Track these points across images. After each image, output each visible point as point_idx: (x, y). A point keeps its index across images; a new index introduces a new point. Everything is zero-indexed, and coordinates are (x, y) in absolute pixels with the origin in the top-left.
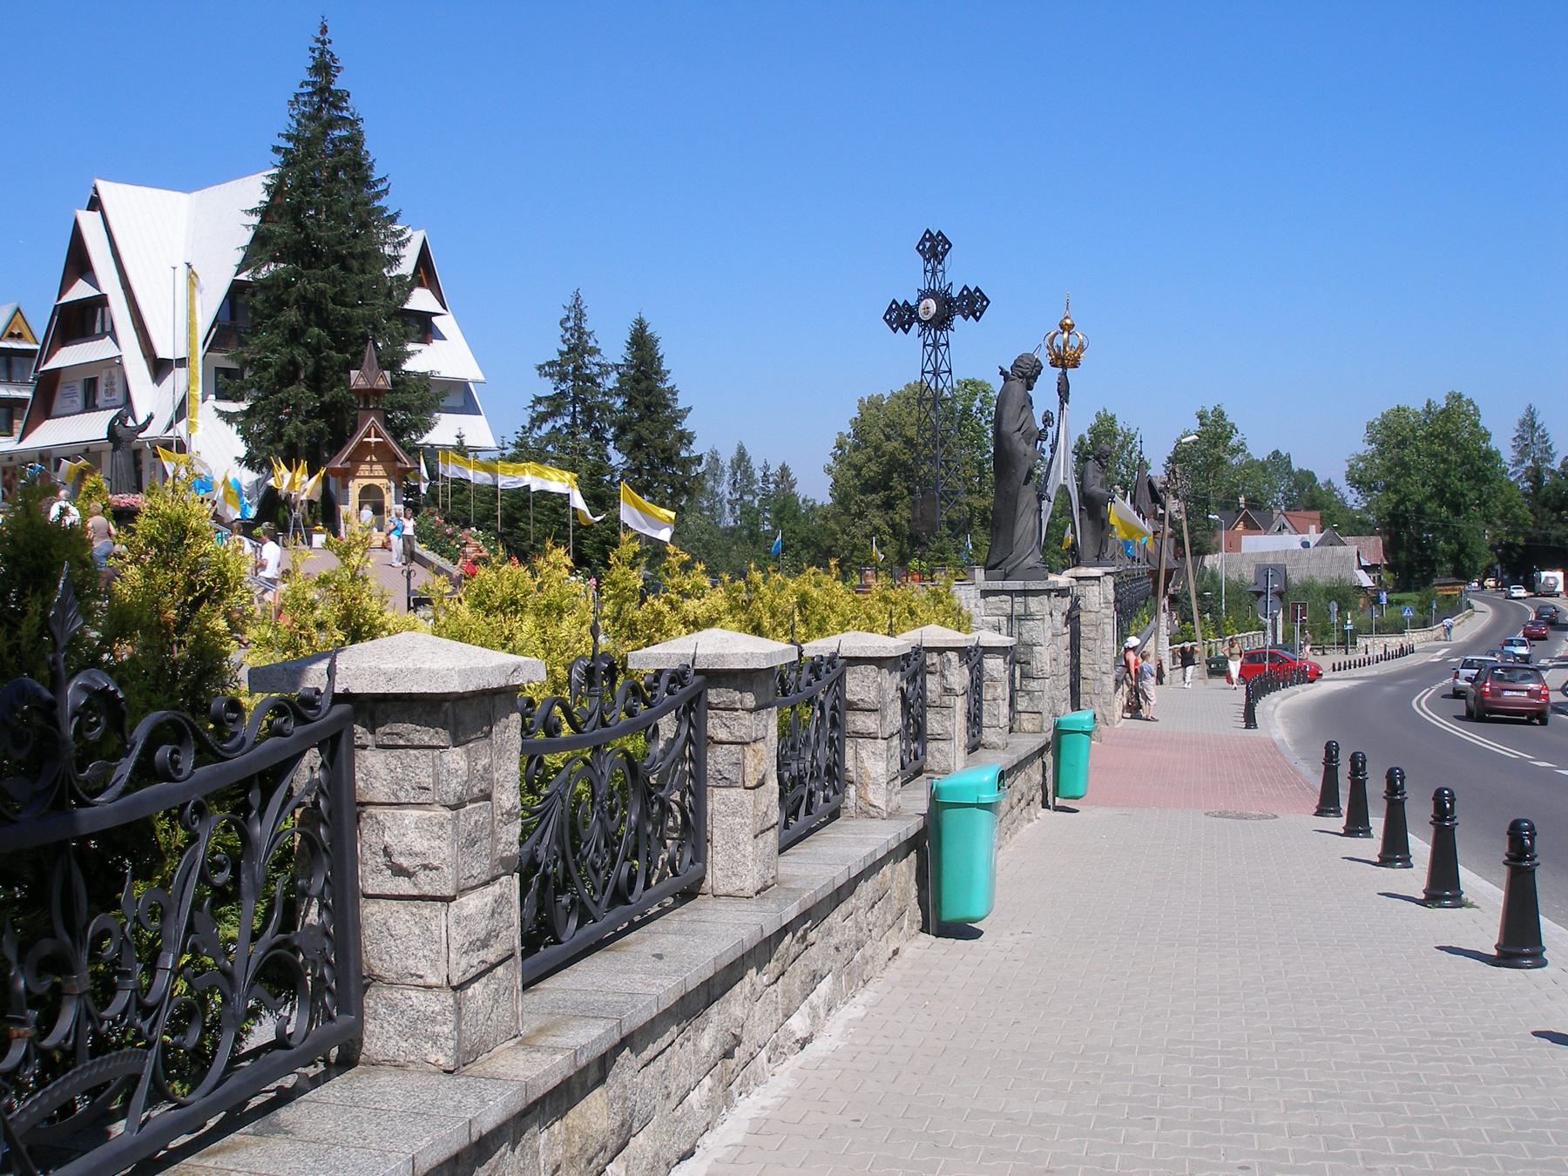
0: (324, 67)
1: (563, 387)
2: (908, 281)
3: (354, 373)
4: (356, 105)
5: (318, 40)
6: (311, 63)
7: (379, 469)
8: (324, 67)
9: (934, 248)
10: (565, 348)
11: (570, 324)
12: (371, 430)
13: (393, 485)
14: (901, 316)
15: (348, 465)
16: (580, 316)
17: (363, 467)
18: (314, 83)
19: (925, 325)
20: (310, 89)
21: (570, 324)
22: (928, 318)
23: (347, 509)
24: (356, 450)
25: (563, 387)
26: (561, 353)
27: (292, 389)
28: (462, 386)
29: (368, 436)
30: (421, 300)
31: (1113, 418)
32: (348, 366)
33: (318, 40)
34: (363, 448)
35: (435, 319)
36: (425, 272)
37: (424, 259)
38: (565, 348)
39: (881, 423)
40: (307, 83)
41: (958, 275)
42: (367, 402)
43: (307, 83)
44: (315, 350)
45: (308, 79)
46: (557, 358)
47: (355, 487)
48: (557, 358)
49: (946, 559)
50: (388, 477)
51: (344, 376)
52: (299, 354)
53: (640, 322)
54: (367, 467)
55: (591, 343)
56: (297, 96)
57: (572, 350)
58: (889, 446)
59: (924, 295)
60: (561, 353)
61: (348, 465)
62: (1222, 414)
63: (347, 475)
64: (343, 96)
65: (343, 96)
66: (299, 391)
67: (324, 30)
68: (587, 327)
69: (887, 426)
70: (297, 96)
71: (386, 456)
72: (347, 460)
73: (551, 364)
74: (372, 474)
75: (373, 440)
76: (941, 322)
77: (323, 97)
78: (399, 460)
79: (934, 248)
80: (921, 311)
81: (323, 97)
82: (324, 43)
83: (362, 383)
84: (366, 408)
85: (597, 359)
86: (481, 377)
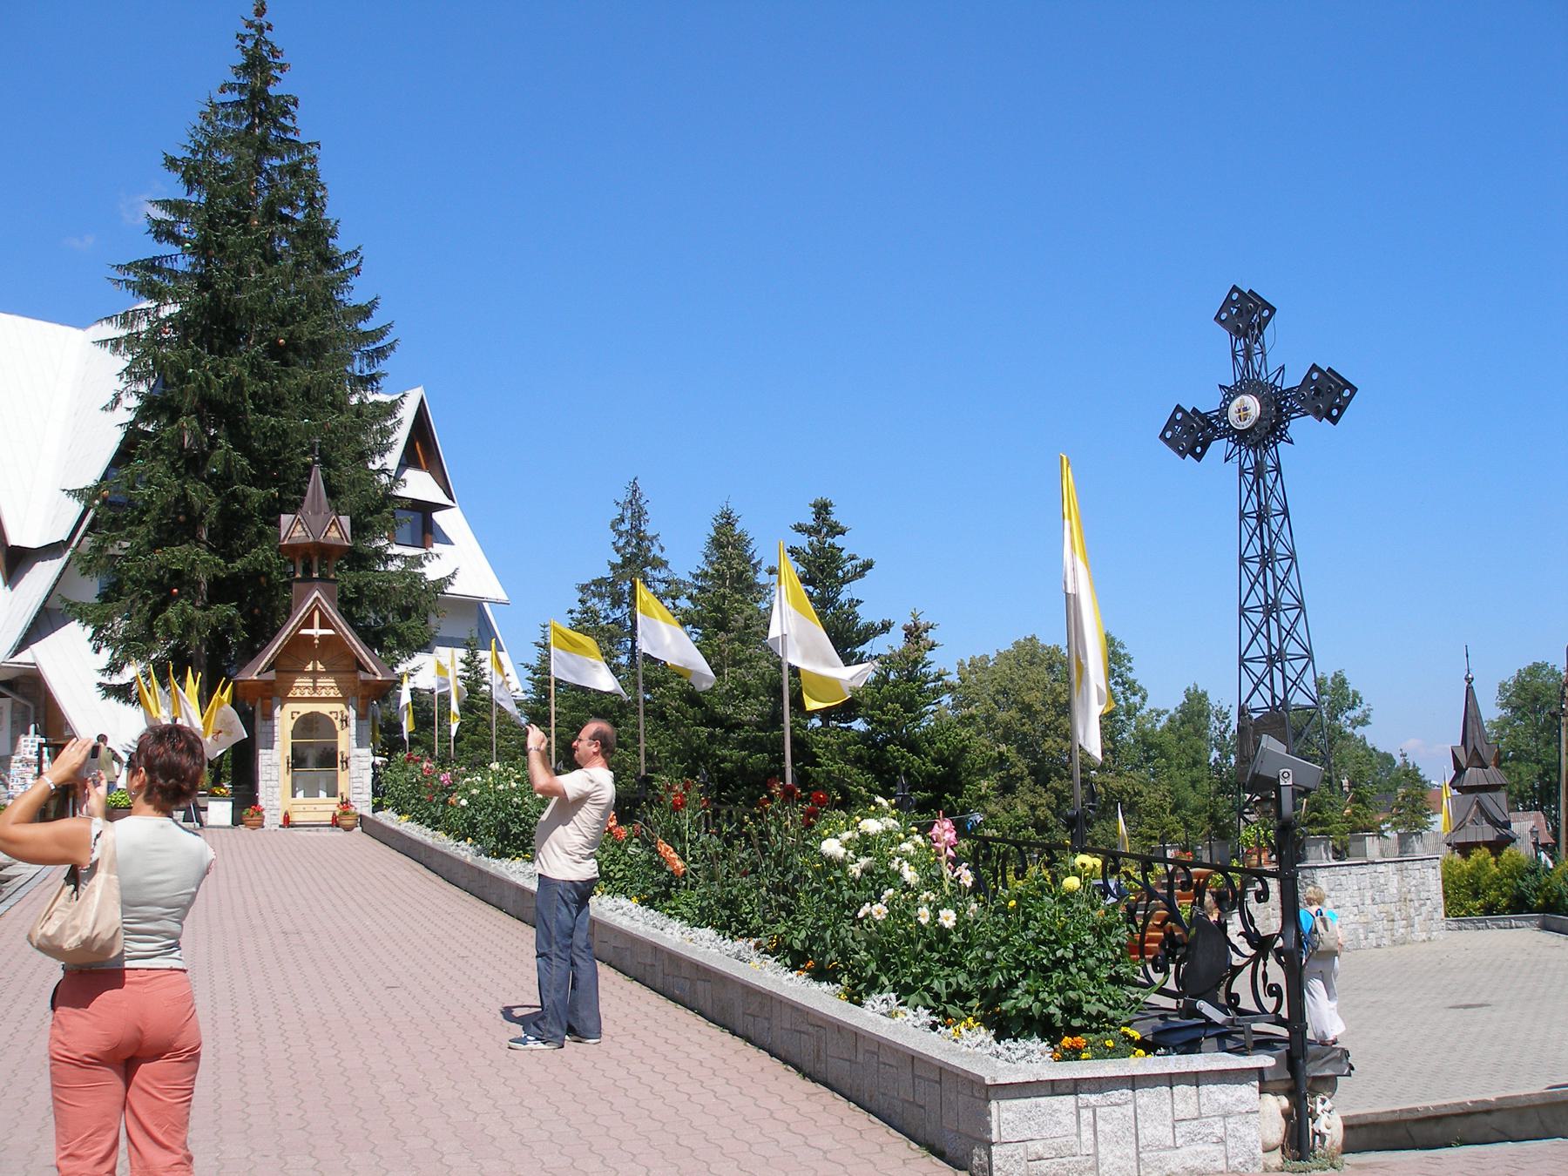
0: (258, 63)
1: (618, 613)
2: (1204, 374)
3: (286, 519)
4: (305, 125)
5: (250, 25)
6: (241, 60)
7: (328, 686)
8: (258, 63)
9: (1246, 315)
10: (618, 560)
11: (626, 526)
12: (314, 613)
13: (352, 713)
14: (1191, 433)
15: (272, 675)
16: (639, 515)
17: (301, 682)
18: (242, 87)
19: (1241, 437)
20: (235, 96)
21: (626, 526)
22: (1246, 425)
23: (273, 764)
24: (287, 650)
25: (618, 613)
26: (614, 567)
27: (181, 551)
28: (473, 607)
29: (308, 623)
30: (419, 485)
31: (1204, 695)
32: (272, 513)
33: (250, 25)
34: (299, 648)
35: (437, 517)
36: (422, 449)
37: (421, 425)
38: (618, 560)
39: (992, 690)
40: (232, 87)
41: (1288, 356)
42: (308, 570)
43: (232, 87)
44: (221, 483)
45: (233, 79)
46: (607, 573)
47: (284, 719)
48: (607, 573)
49: (1324, 822)
50: (343, 700)
51: (269, 530)
52: (197, 492)
53: (727, 521)
54: (307, 682)
55: (655, 551)
56: (214, 107)
57: (627, 562)
58: (1002, 716)
59: (1231, 393)
60: (614, 567)
61: (272, 675)
62: (1343, 681)
63: (273, 693)
64: (285, 106)
65: (285, 106)
66: (198, 559)
67: (260, 12)
68: (649, 529)
69: (998, 692)
70: (214, 107)
71: (334, 655)
72: (271, 666)
73: (599, 583)
74: (316, 695)
75: (316, 631)
76: (1268, 432)
77: (258, 105)
78: (361, 667)
79: (1246, 315)
80: (1232, 415)
81: (258, 105)
82: (261, 29)
83: (299, 534)
84: (308, 578)
85: (663, 574)
86: (503, 597)
